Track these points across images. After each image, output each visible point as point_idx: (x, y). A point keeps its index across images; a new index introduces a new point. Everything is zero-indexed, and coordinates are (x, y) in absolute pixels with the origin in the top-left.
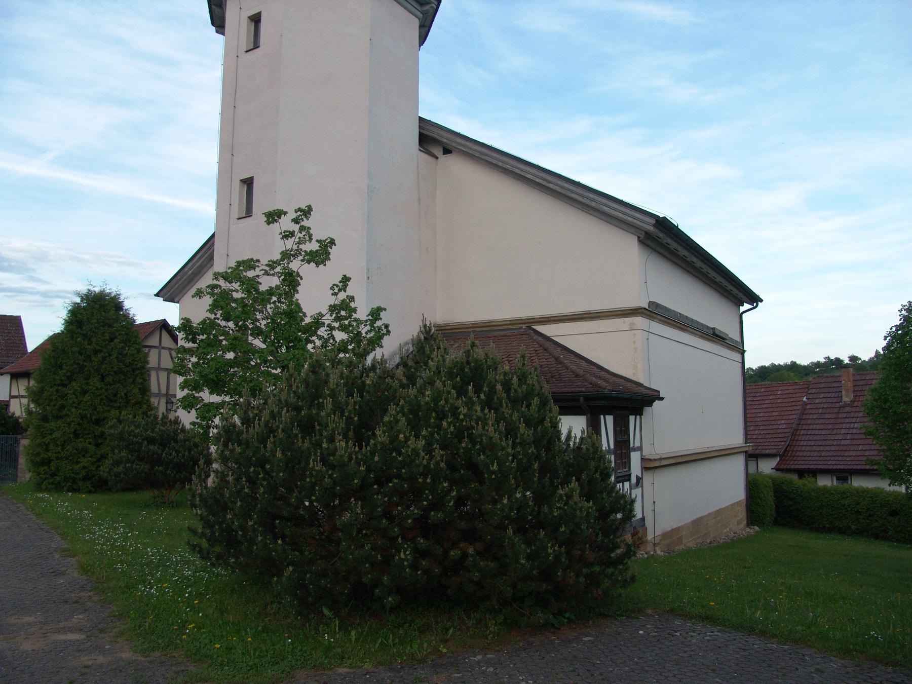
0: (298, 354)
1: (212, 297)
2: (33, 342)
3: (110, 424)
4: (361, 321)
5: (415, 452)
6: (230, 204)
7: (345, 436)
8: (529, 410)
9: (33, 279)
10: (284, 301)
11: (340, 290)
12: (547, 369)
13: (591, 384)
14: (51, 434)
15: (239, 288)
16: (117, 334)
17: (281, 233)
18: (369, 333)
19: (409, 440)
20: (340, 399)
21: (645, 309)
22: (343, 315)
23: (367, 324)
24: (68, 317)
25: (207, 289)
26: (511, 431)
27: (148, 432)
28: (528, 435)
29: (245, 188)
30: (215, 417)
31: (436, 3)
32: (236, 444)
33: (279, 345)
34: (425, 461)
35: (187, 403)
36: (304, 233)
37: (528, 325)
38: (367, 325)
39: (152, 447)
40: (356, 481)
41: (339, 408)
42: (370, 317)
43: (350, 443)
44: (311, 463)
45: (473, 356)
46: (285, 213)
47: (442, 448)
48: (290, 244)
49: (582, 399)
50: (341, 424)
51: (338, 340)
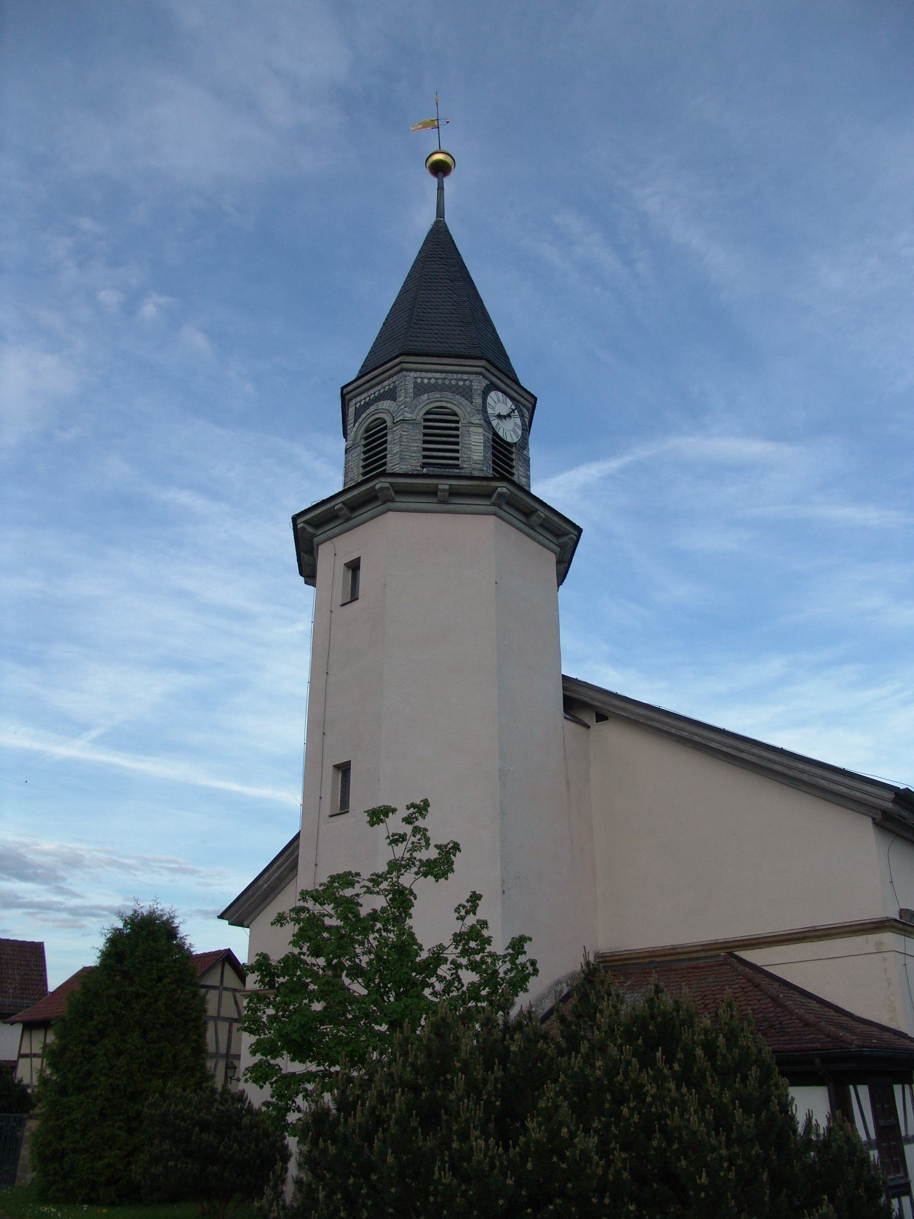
0: (412, 1004)
1: (297, 924)
2: (55, 979)
3: (151, 1100)
4: (497, 956)
5: (585, 1156)
6: (321, 798)
7: (485, 1133)
8: (745, 1087)
9: (61, 891)
10: (392, 928)
11: (467, 913)
12: (760, 1015)
13: (829, 1036)
14: (69, 1114)
15: (332, 912)
16: (168, 972)
17: (388, 837)
18: (509, 973)
19: (575, 1137)
20: (475, 1074)
21: (896, 920)
22: (472, 947)
23: (507, 959)
24: (106, 947)
25: (291, 914)
26: (722, 1121)
27: (202, 1114)
28: (749, 1126)
29: (340, 775)
30: (297, 1095)
31: (576, 533)
32: (329, 1141)
33: (385, 990)
34: (600, 1169)
35: (259, 1074)
36: (418, 836)
37: (728, 951)
38: (506, 961)
39: (205, 1136)
40: (501, 1202)
41: (474, 1088)
42: (510, 951)
43: (492, 1141)
44: (437, 1173)
45: (659, 1006)
46: (394, 811)
47: (623, 1149)
48: (400, 851)
49: (817, 1061)
50: (478, 1112)
51: (465, 981)
